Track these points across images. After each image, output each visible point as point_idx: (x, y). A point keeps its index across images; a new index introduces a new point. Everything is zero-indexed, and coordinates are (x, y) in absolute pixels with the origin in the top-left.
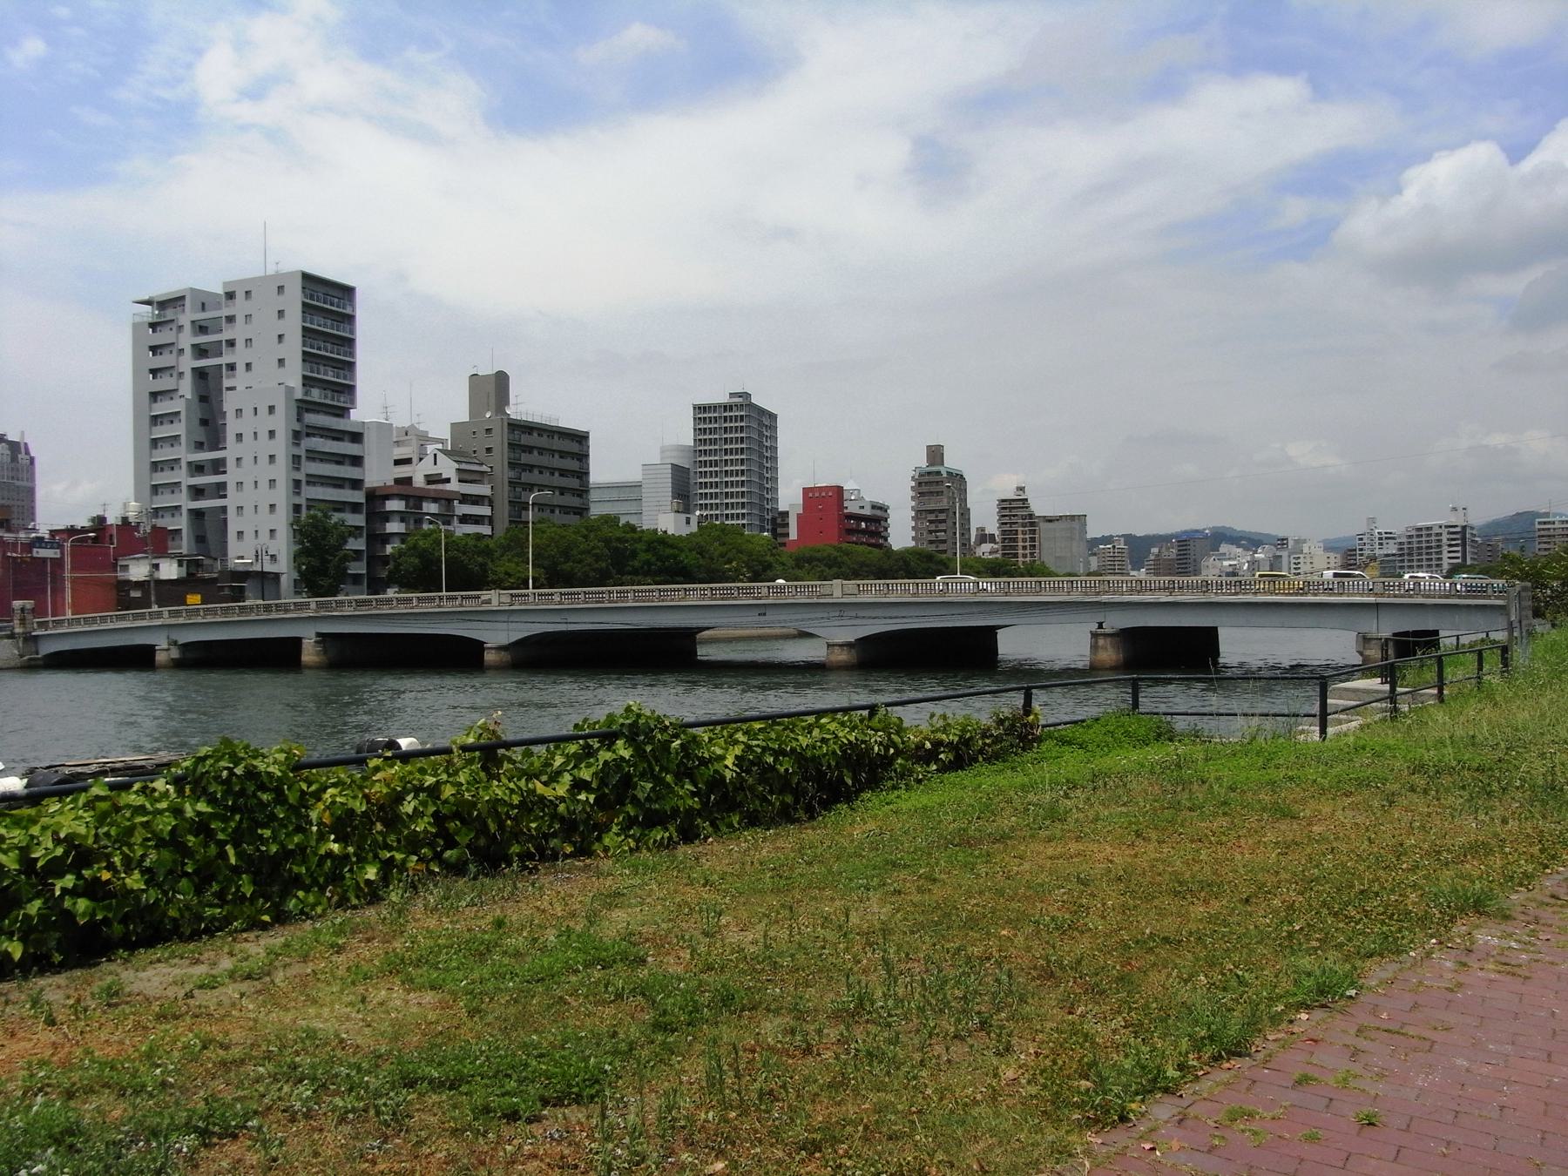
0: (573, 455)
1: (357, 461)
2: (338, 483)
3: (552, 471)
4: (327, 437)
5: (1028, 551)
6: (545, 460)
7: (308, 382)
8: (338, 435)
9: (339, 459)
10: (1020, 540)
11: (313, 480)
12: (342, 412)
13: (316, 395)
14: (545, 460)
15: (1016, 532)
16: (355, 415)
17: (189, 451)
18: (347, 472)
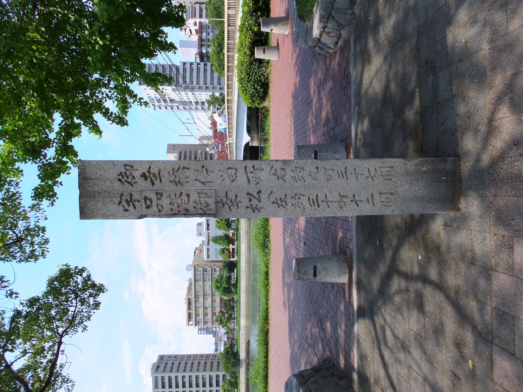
8: (185, 70)
9: (191, 70)
16: (178, 64)
18: (195, 67)
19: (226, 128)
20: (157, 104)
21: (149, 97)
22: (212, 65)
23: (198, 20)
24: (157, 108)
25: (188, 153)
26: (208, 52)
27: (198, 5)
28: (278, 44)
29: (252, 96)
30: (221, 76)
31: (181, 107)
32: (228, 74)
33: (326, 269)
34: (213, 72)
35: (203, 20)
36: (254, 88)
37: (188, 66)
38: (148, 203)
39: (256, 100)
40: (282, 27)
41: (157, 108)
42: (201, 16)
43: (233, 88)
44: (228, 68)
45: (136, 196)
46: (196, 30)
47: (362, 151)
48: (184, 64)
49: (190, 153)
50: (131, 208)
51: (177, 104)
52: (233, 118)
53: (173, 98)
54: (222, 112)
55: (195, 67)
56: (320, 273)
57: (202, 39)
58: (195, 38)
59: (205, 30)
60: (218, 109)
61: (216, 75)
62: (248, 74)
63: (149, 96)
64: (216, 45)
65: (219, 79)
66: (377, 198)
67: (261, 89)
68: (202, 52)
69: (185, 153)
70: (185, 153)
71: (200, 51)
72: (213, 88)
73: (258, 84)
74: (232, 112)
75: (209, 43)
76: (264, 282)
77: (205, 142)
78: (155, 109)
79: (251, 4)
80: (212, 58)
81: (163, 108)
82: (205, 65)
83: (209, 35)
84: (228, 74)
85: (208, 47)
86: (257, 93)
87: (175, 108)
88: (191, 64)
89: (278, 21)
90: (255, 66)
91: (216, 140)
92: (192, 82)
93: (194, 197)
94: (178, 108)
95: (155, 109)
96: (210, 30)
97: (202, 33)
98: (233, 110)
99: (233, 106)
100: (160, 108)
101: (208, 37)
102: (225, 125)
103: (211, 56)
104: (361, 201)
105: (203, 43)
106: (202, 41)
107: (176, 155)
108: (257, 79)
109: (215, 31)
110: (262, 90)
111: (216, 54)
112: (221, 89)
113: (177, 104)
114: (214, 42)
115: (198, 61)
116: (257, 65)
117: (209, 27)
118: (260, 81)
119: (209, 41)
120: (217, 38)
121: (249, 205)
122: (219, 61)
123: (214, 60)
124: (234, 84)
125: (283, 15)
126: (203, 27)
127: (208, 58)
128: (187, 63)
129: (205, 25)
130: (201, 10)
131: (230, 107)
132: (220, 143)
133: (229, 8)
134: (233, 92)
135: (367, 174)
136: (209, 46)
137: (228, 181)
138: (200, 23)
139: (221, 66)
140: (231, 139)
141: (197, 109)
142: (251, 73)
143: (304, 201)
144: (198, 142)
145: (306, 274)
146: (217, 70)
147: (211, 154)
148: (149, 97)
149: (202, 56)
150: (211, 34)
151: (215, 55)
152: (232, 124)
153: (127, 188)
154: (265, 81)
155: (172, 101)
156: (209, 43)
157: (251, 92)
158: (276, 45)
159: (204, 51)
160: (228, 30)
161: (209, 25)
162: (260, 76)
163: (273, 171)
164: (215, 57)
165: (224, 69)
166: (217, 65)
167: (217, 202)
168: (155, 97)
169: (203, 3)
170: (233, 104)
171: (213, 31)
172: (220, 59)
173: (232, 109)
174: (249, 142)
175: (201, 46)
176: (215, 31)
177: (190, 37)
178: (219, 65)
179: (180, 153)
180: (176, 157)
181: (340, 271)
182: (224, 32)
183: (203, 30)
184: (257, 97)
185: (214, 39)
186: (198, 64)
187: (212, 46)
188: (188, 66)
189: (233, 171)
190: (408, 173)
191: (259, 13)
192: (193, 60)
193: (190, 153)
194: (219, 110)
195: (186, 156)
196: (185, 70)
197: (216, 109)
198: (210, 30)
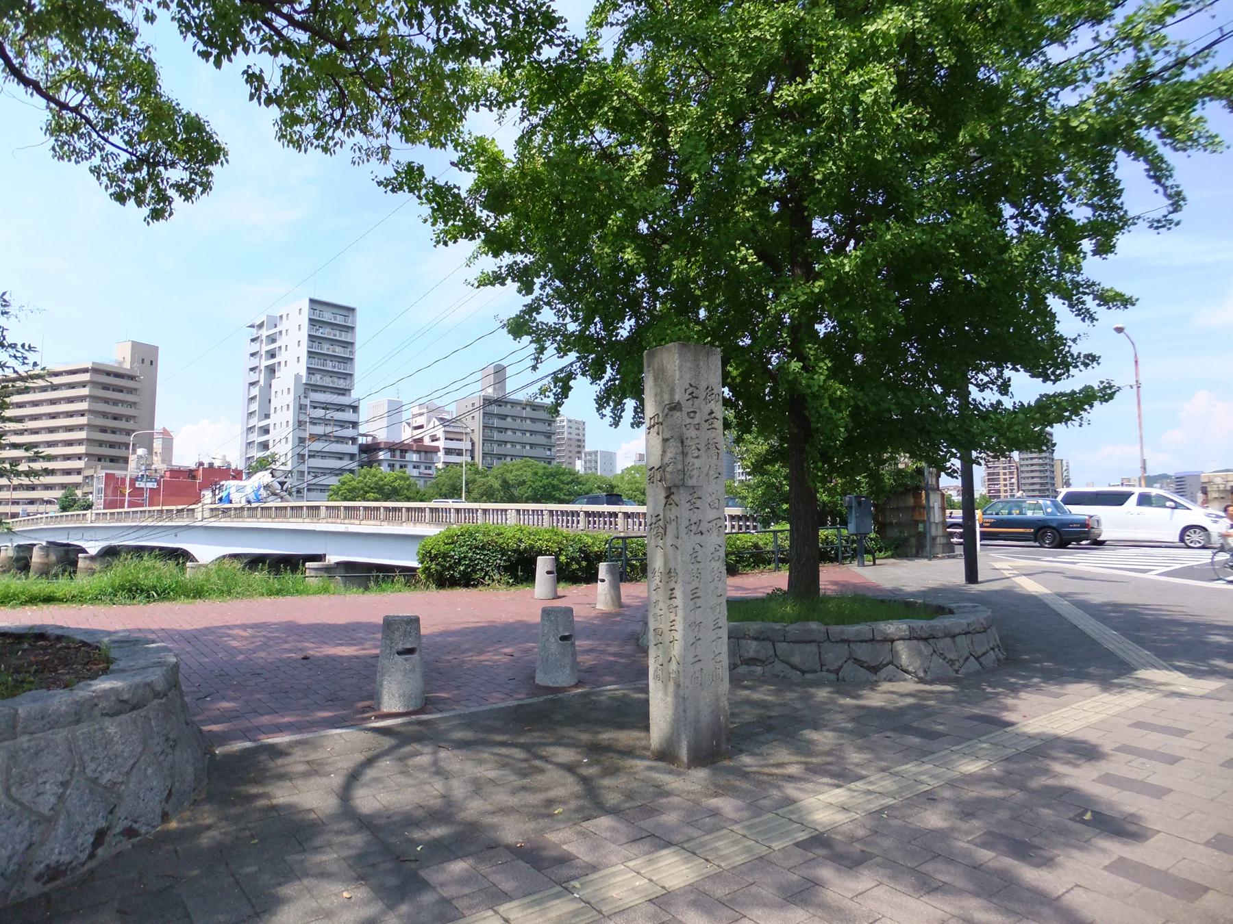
0: (491, 428)
1: (355, 425)
2: (341, 440)
3: (524, 432)
4: (335, 393)
5: (1008, 488)
6: (517, 424)
7: (311, 371)
8: (341, 408)
9: (342, 424)
10: (1001, 480)
11: (314, 421)
12: (344, 392)
13: (317, 379)
14: (517, 424)
15: (998, 474)
16: (355, 394)
17: (259, 436)
18: (349, 432)
19: (231, 502)
20: (264, 333)
21: (281, 317)
22: (352, 471)
23: (441, 444)
24: (254, 333)
25: (130, 398)
26: (380, 465)
27: (470, 447)
28: (559, 597)
29: (445, 556)
30: (331, 493)
31: (255, 391)
32: (382, 510)
33: (412, 670)
34: (337, 475)
35: (441, 454)
36: (460, 559)
37: (348, 416)
38: (692, 415)
39: (437, 564)
40: (609, 597)
41: (254, 333)
42: (448, 451)
43: (346, 521)
44: (395, 509)
45: (697, 402)
46: (421, 440)
47: (640, 684)
48: (355, 409)
49: (132, 404)
50: (687, 397)
51: (262, 383)
52: (270, 520)
53: (277, 374)
54: (274, 494)
55: (349, 432)
56: (406, 660)
57: (406, 451)
58: (406, 435)
59: (423, 460)
60: (282, 484)
61: (333, 481)
62: (483, 548)
63: (284, 317)
64: (396, 484)
65: (323, 489)
66: (698, 666)
67: (460, 573)
68: (381, 450)
69: (131, 391)
70: (131, 391)
71: (382, 446)
72: (302, 473)
73: (468, 566)
74: (285, 517)
75: (397, 467)
76: (23, 593)
77: (157, 445)
78: (252, 326)
79: (596, 549)
80: (368, 473)
81: (255, 347)
82: (352, 456)
83: (414, 467)
84: (382, 510)
85: (389, 465)
86: (450, 565)
87: (254, 377)
88: (355, 425)
89: (616, 588)
90: (500, 559)
91: (168, 474)
92: (315, 424)
93: (697, 463)
94: (252, 384)
95: (252, 326)
96: (422, 470)
97: (418, 452)
98: (291, 520)
99: (301, 520)
100: (253, 340)
101: (410, 466)
102: (238, 500)
103: (373, 469)
104: (696, 648)
105: (398, 453)
106: (402, 451)
107: (127, 365)
108: (477, 565)
109: (422, 480)
110: (456, 574)
111: (376, 483)
112: (298, 492)
113: (262, 383)
114: (402, 478)
115: (362, 440)
116: (502, 563)
117: (430, 468)
118: (474, 571)
119: (401, 467)
120: (409, 485)
121: (692, 522)
122: (362, 488)
123: (365, 478)
124: (357, 522)
125: (624, 600)
126: (429, 455)
127: (370, 464)
128: (356, 415)
129: (432, 459)
130: (459, 453)
131: (283, 512)
132: (159, 484)
133: (518, 511)
134: (339, 521)
135: (717, 652)
136: (392, 466)
137: (709, 500)
138: (436, 450)
139: (352, 494)
140: (207, 514)
141: (250, 429)
142: (485, 552)
143: (695, 584)
144: (158, 426)
145: (405, 635)
146: (343, 483)
147: (126, 460)
148: (281, 317)
149: (370, 450)
150: (415, 472)
151: (375, 479)
152: (249, 517)
153: (702, 395)
154: (474, 580)
155: (271, 370)
156: (397, 467)
157: (453, 553)
158: (559, 594)
159: (382, 455)
160: (477, 510)
161: (433, 468)
162: (482, 569)
163: (718, 548)
164: (370, 481)
165: (345, 499)
166: (354, 483)
167: (693, 487)
168: (281, 332)
169: (473, 458)
170: (306, 520)
171: (420, 477)
172: (367, 492)
173: (262, 517)
174: (197, 561)
175: (392, 448)
176: (422, 480)
177: (409, 424)
178: (351, 490)
179: (132, 378)
180: (121, 363)
181: (410, 696)
182: (421, 501)
183: (423, 454)
184: (442, 566)
185: (408, 479)
186: (354, 440)
187: (394, 474)
188: (348, 416)
189: (716, 505)
190: (718, 699)
191: (584, 563)
192: (362, 429)
193: (132, 404)
194: (280, 487)
195: (121, 391)
196: (341, 408)
197: (282, 479)
198: (422, 470)
